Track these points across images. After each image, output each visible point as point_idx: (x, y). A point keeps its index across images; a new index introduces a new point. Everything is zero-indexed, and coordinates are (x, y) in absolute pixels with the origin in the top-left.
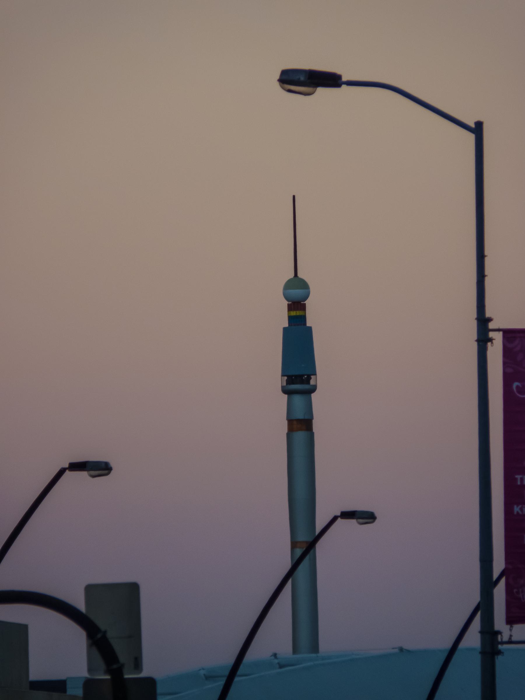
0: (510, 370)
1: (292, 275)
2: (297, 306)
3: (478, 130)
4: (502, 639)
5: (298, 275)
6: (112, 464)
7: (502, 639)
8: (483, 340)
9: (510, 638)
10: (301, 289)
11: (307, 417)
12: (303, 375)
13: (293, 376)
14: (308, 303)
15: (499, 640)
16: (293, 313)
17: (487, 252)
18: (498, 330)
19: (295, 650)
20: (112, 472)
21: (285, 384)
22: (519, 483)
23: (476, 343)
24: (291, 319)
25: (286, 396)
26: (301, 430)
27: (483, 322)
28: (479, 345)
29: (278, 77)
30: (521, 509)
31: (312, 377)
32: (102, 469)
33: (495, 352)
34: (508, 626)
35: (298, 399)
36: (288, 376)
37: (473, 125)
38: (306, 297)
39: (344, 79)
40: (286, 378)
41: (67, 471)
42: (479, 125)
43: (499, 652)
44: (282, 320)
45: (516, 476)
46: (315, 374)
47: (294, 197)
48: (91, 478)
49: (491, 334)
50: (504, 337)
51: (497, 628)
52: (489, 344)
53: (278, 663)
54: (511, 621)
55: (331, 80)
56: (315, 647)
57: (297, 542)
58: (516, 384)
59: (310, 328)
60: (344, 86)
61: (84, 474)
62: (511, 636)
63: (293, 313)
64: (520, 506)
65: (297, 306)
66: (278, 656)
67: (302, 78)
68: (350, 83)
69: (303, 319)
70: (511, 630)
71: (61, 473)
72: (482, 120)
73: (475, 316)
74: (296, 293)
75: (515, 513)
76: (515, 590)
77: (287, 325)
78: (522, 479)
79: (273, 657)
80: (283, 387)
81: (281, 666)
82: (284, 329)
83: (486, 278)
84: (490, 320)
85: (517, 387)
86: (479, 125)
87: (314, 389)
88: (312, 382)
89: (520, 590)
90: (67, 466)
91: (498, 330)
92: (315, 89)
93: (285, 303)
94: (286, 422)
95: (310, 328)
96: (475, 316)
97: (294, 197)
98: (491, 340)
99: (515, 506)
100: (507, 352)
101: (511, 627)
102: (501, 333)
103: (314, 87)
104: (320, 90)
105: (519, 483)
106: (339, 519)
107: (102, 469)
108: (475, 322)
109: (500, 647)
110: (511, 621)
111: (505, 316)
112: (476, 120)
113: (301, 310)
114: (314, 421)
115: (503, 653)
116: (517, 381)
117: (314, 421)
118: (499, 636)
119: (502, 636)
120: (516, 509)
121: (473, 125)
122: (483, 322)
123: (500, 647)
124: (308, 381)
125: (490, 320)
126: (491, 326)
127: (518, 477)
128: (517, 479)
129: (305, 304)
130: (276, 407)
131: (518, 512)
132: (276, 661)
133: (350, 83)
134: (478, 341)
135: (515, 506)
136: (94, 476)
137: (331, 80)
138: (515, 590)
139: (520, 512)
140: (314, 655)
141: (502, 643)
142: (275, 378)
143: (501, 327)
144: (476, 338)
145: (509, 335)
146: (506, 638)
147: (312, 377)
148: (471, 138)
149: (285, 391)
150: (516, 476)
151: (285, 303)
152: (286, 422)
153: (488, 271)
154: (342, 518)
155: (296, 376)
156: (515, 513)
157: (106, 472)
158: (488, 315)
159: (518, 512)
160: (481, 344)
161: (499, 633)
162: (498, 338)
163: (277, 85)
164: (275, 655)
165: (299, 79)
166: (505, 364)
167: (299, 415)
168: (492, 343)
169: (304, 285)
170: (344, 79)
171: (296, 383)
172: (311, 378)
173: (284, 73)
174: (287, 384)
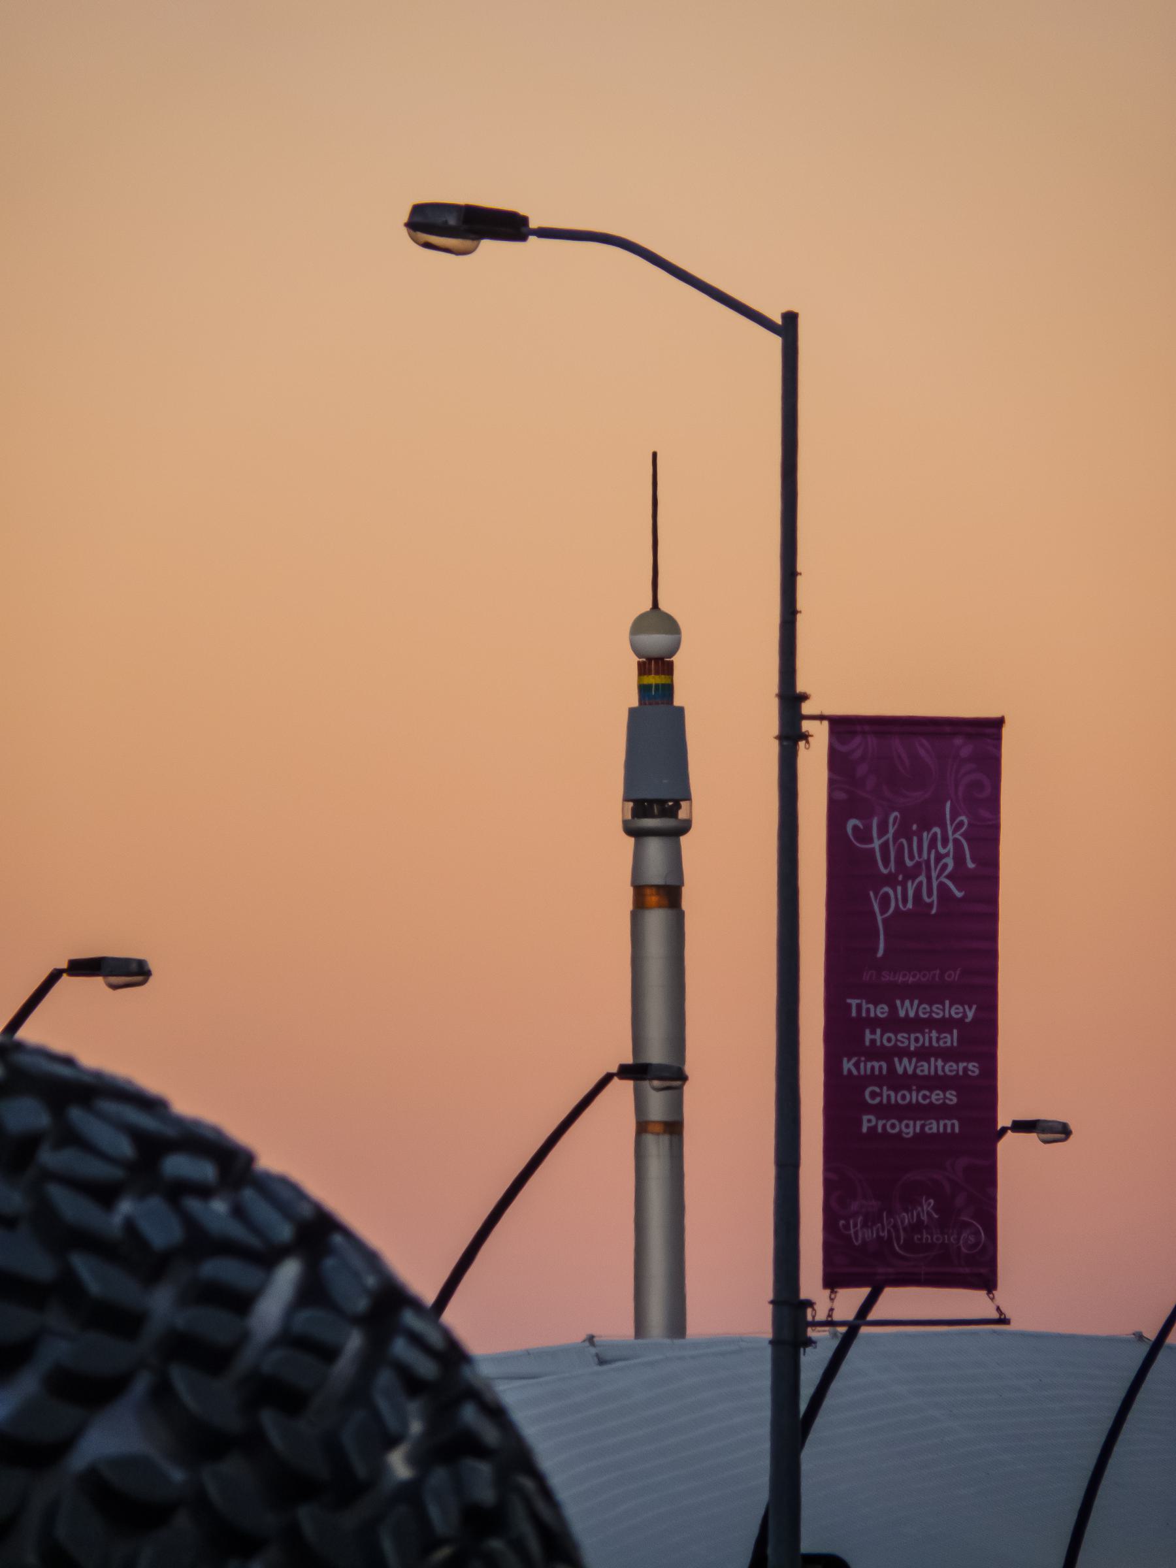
0: (841, 796)
1: (648, 605)
2: (656, 671)
4: (814, 1317)
5: (660, 606)
6: (152, 966)
7: (814, 1317)
8: (791, 736)
9: (830, 1315)
10: (658, 632)
11: (670, 882)
12: (667, 801)
13: (644, 800)
14: (679, 661)
15: (809, 1318)
16: (652, 680)
18: (821, 718)
20: (151, 979)
21: (629, 816)
22: (854, 1014)
23: (776, 743)
24: (643, 690)
25: (632, 840)
26: (660, 906)
27: (791, 700)
28: (781, 745)
29: (405, 218)
30: (857, 1065)
31: (683, 803)
32: (129, 972)
34: (828, 1292)
35: (654, 846)
36: (635, 801)
39: (533, 224)
40: (631, 804)
41: (65, 975)
42: (791, 319)
47: (655, 455)
48: (110, 990)
49: (806, 726)
50: (833, 732)
51: (804, 1295)
52: (802, 744)
54: (833, 1281)
55: (508, 226)
56: (677, 1325)
58: (852, 822)
59: (681, 710)
61: (98, 982)
62: (832, 1310)
63: (652, 680)
64: (854, 1060)
65: (656, 671)
66: (595, 1339)
67: (452, 221)
69: (667, 691)
71: (54, 978)
74: (655, 641)
75: (845, 1072)
77: (635, 703)
78: (859, 1007)
79: (587, 1344)
80: (625, 822)
81: (602, 1362)
82: (632, 711)
84: (804, 697)
85: (855, 828)
86: (791, 319)
87: (685, 827)
88: (682, 814)
89: (851, 1222)
90: (65, 966)
91: (821, 718)
94: (631, 890)
95: (681, 710)
96: (775, 689)
97: (655, 455)
98: (805, 737)
99: (845, 1060)
100: (837, 761)
102: (826, 723)
103: (473, 239)
104: (487, 245)
105: (854, 1014)
106: (616, 1080)
107: (129, 972)
111: (829, 692)
112: (784, 310)
113: (663, 673)
114: (685, 891)
116: (856, 818)
118: (809, 1311)
120: (847, 1065)
122: (791, 700)
124: (672, 812)
125: (804, 697)
126: (807, 708)
127: (854, 1002)
128: (850, 1005)
129: (672, 663)
130: (610, 858)
131: (849, 1071)
132: (593, 1350)
134: (782, 738)
135: (845, 1060)
137: (508, 226)
138: (842, 1222)
140: (678, 1342)
143: (827, 712)
146: (821, 1316)
147: (683, 803)
148: (775, 343)
149: (630, 831)
150: (849, 1001)
151: (634, 660)
152: (631, 889)
153: (802, 602)
156: (845, 1072)
157: (140, 978)
158: (801, 687)
159: (849, 1071)
161: (809, 1304)
162: (819, 734)
163: (404, 231)
164: (591, 1339)
165: (446, 222)
166: (832, 783)
167: (656, 874)
168: (808, 742)
169: (670, 626)
170: (533, 224)
172: (679, 807)
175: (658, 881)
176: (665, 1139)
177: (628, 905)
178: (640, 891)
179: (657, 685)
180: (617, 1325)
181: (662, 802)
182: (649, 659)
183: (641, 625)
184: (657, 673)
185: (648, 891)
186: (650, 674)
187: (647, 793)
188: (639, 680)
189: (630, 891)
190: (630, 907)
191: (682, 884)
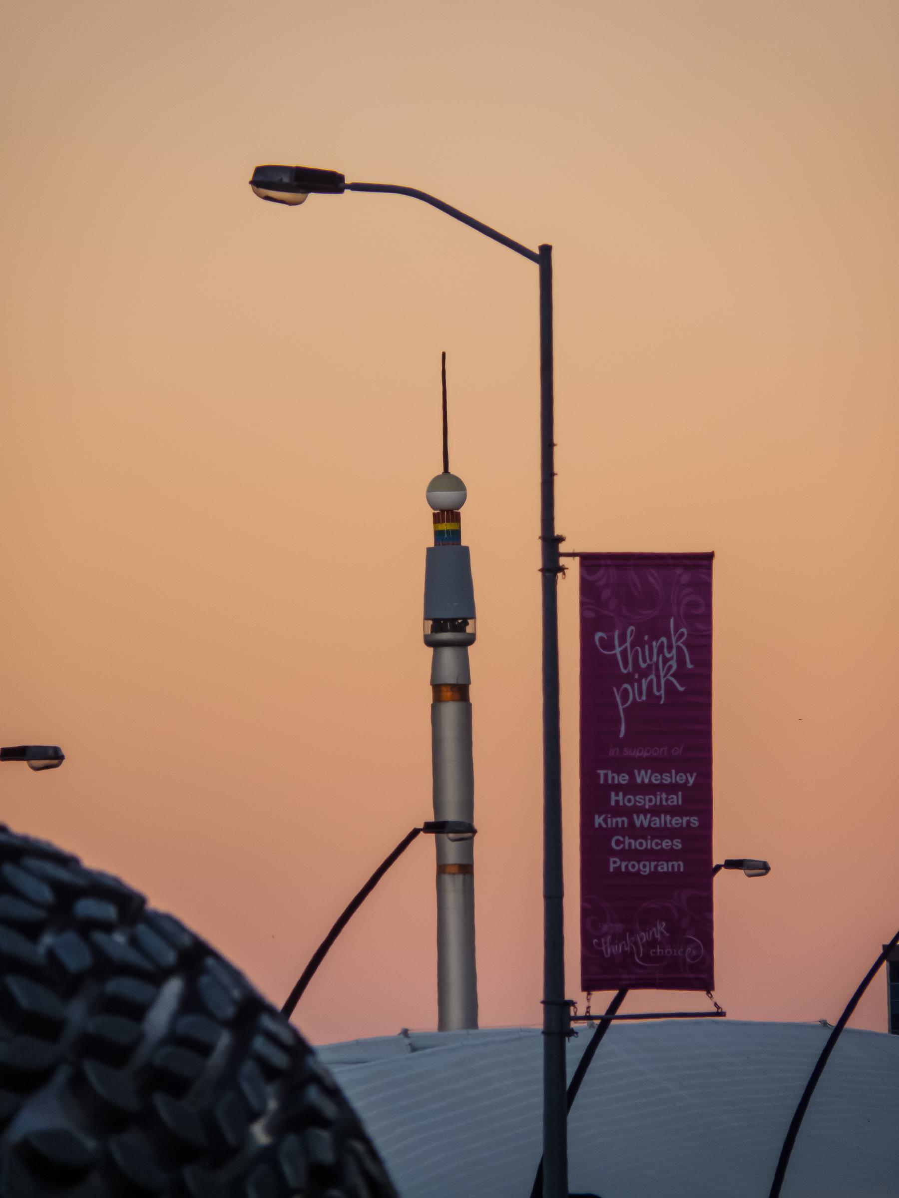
0: (590, 615)
1: (440, 471)
2: (447, 517)
4: (575, 1013)
5: (450, 470)
6: (64, 751)
7: (575, 1013)
8: (551, 569)
9: (588, 1012)
11: (461, 682)
12: (457, 619)
14: (462, 511)
15: (572, 1014)
16: (444, 527)
17: (557, 438)
18: (573, 555)
19: (442, 1024)
20: (64, 762)
22: (602, 781)
24: (438, 534)
25: (431, 650)
26: (453, 700)
27: (551, 542)
29: (250, 178)
30: (605, 820)
33: (569, 588)
34: (585, 994)
35: (448, 654)
36: (435, 620)
37: (537, 252)
39: (348, 181)
40: (430, 623)
42: (546, 250)
44: (424, 535)
45: (599, 771)
46: (473, 617)
47: (444, 354)
49: (563, 561)
50: (583, 565)
51: (568, 996)
52: (560, 575)
53: (410, 1045)
54: (589, 985)
55: (330, 182)
56: (471, 1019)
57: (445, 866)
58: (598, 635)
60: (347, 192)
62: (588, 1008)
63: (444, 527)
64: (603, 816)
65: (447, 517)
67: (286, 180)
69: (456, 535)
70: (588, 1000)
72: (549, 243)
74: (446, 497)
75: (597, 825)
77: (432, 544)
79: (402, 1036)
80: (426, 636)
83: (556, 478)
84: (561, 539)
85: (601, 639)
87: (471, 640)
88: (469, 629)
89: (603, 940)
91: (573, 555)
92: (304, 195)
93: (428, 513)
94: (430, 688)
95: (466, 549)
97: (444, 354)
98: (562, 569)
99: (597, 816)
100: (587, 589)
101: (589, 994)
102: (577, 559)
104: (314, 198)
105: (602, 781)
106: (422, 833)
110: (589, 985)
111: (581, 534)
112: (541, 243)
113: (453, 521)
115: (577, 1033)
117: (471, 687)
118: (572, 1008)
122: (551, 542)
124: (461, 628)
125: (561, 539)
126: (563, 548)
127: (602, 772)
129: (459, 514)
132: (407, 1041)
134: (544, 570)
135: (597, 816)
136: (37, 769)
137: (330, 182)
138: (595, 941)
139: (604, 825)
140: (472, 1032)
141: (577, 1018)
142: (416, 624)
143: (577, 551)
144: (539, 565)
145: (589, 561)
146: (581, 1012)
147: (470, 621)
148: (534, 269)
149: (429, 642)
150: (599, 771)
155: (446, 620)
156: (597, 825)
157: (55, 762)
158: (558, 531)
159: (600, 824)
160: (547, 574)
161: (572, 1003)
162: (573, 567)
164: (405, 1033)
165: (281, 180)
166: (583, 604)
167: (449, 675)
168: (564, 574)
169: (458, 485)
170: (348, 181)
171: (446, 631)
172: (467, 624)
175: (452, 681)
176: (460, 878)
177: (430, 699)
178: (437, 688)
179: (448, 531)
180: (424, 1019)
181: (453, 620)
182: (443, 511)
183: (435, 485)
184: (448, 522)
185: (444, 689)
186: (443, 522)
187: (445, 614)
188: (435, 527)
189: (430, 689)
190: (431, 701)
191: (470, 683)
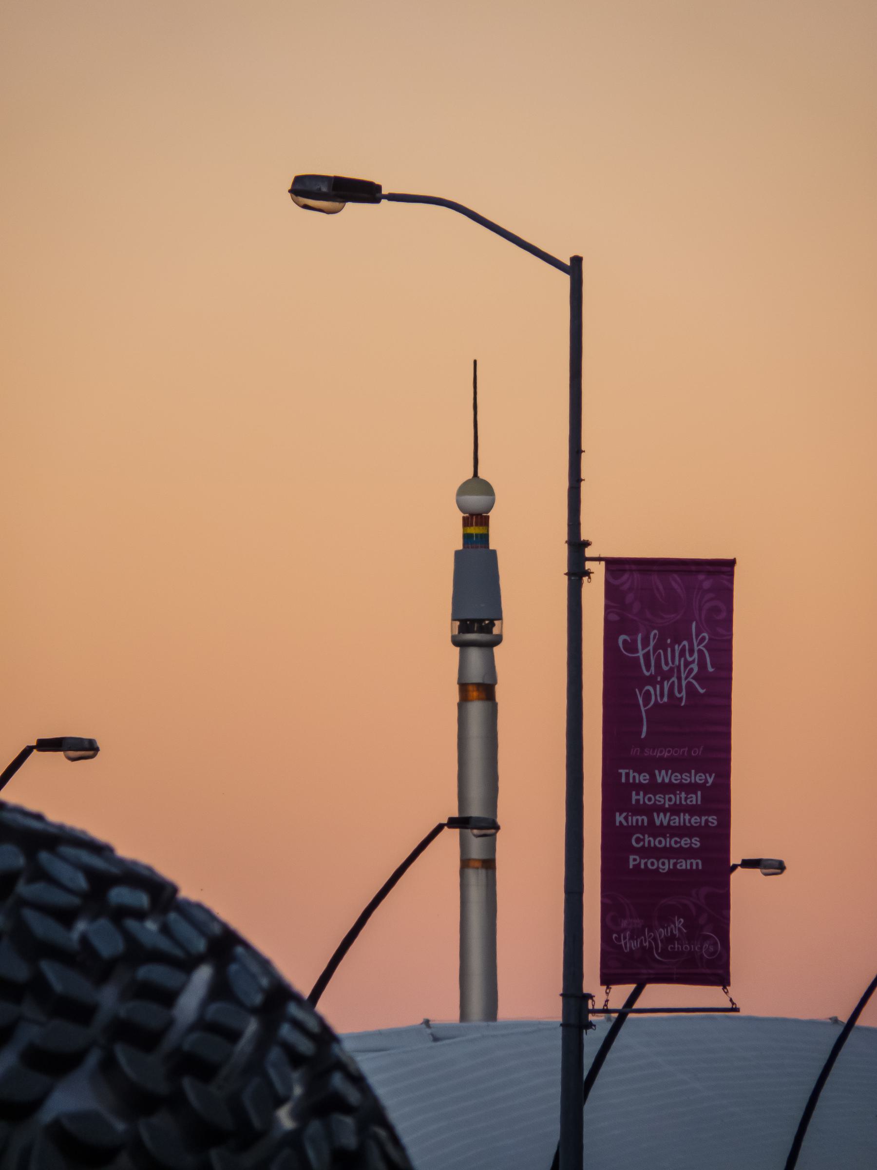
0: (614, 617)
1: (470, 475)
2: (476, 521)
3: (574, 269)
8: (577, 573)
9: (606, 1005)
12: (484, 620)
13: (466, 620)
15: (590, 1007)
18: (599, 559)
22: (623, 780)
24: (467, 538)
25: (458, 649)
26: (479, 699)
27: (577, 546)
28: (569, 579)
30: (626, 818)
32: (83, 748)
34: (605, 987)
35: (475, 654)
38: (490, 508)
40: (458, 623)
42: (577, 261)
43: (590, 1025)
45: (620, 771)
46: (500, 618)
47: (475, 362)
48: (69, 762)
49: (589, 565)
50: (607, 569)
51: (586, 989)
52: (585, 579)
54: (608, 979)
55: (366, 192)
57: (469, 860)
60: (384, 201)
64: (624, 814)
65: (476, 521)
67: (324, 189)
68: (393, 197)
70: (607, 994)
71: (26, 753)
73: (566, 538)
74: (476, 501)
76: (614, 936)
77: (460, 547)
79: (424, 1026)
81: (436, 1039)
82: (457, 553)
83: (583, 484)
84: (587, 544)
85: (625, 641)
86: (577, 261)
87: (498, 640)
88: (496, 631)
91: (599, 559)
92: (342, 204)
93: (458, 517)
96: (565, 537)
97: (475, 362)
98: (588, 573)
99: (617, 814)
102: (603, 563)
103: (340, 202)
104: (351, 207)
105: (623, 780)
107: (83, 748)
108: (565, 547)
109: (591, 1018)
111: (607, 540)
112: (572, 255)
113: (481, 525)
118: (590, 1002)
119: (593, 1001)
121: (568, 263)
122: (577, 546)
123: (591, 1018)
124: (488, 629)
125: (587, 544)
126: (589, 552)
127: (623, 772)
128: (621, 774)
132: (429, 1031)
133: (393, 197)
134: (569, 574)
135: (617, 814)
136: (74, 759)
137: (366, 192)
138: (614, 936)
140: (491, 1024)
141: (595, 1012)
142: (444, 625)
146: (599, 1005)
147: (496, 622)
148: (565, 279)
149: (456, 642)
150: (620, 771)
154: (450, 827)
155: (473, 621)
156: (617, 824)
157: (91, 753)
158: (584, 536)
161: (590, 997)
162: (598, 570)
164: (427, 1022)
165: (320, 189)
167: (476, 675)
168: (590, 578)
169: (487, 489)
170: (385, 191)
172: (494, 625)
173: (298, 180)
174: (459, 632)
